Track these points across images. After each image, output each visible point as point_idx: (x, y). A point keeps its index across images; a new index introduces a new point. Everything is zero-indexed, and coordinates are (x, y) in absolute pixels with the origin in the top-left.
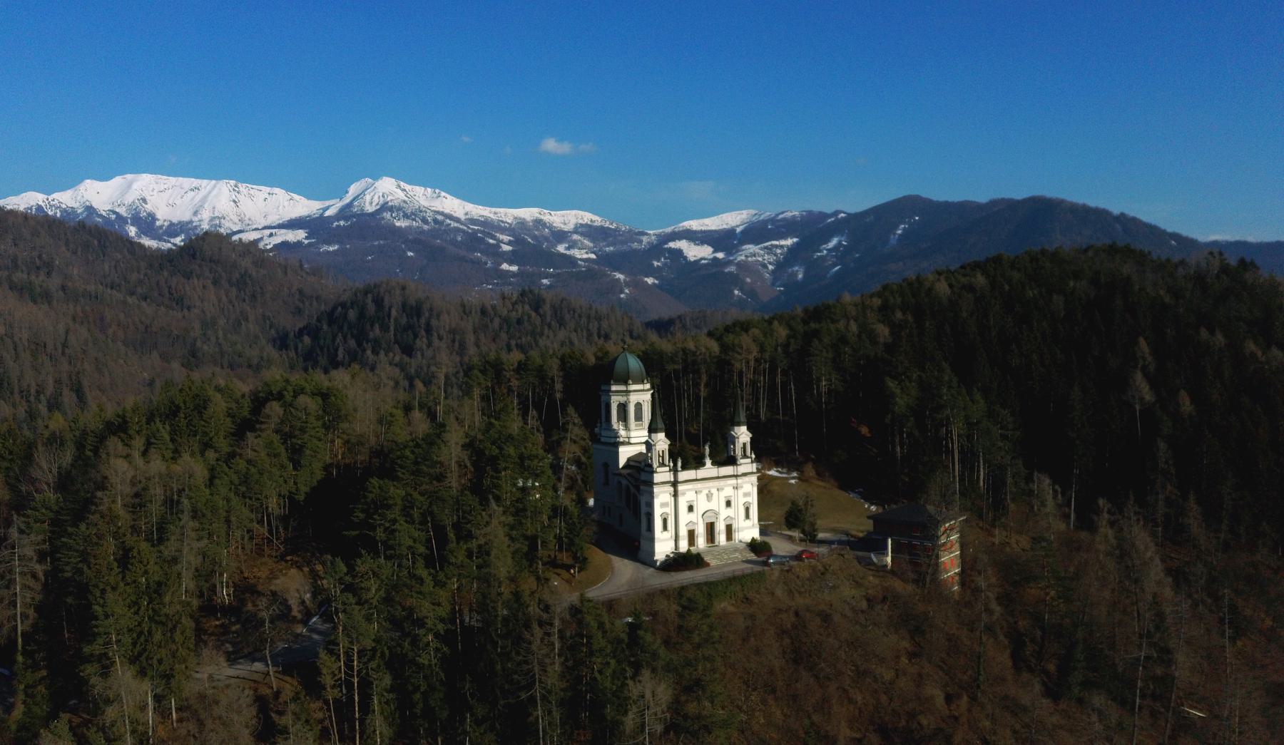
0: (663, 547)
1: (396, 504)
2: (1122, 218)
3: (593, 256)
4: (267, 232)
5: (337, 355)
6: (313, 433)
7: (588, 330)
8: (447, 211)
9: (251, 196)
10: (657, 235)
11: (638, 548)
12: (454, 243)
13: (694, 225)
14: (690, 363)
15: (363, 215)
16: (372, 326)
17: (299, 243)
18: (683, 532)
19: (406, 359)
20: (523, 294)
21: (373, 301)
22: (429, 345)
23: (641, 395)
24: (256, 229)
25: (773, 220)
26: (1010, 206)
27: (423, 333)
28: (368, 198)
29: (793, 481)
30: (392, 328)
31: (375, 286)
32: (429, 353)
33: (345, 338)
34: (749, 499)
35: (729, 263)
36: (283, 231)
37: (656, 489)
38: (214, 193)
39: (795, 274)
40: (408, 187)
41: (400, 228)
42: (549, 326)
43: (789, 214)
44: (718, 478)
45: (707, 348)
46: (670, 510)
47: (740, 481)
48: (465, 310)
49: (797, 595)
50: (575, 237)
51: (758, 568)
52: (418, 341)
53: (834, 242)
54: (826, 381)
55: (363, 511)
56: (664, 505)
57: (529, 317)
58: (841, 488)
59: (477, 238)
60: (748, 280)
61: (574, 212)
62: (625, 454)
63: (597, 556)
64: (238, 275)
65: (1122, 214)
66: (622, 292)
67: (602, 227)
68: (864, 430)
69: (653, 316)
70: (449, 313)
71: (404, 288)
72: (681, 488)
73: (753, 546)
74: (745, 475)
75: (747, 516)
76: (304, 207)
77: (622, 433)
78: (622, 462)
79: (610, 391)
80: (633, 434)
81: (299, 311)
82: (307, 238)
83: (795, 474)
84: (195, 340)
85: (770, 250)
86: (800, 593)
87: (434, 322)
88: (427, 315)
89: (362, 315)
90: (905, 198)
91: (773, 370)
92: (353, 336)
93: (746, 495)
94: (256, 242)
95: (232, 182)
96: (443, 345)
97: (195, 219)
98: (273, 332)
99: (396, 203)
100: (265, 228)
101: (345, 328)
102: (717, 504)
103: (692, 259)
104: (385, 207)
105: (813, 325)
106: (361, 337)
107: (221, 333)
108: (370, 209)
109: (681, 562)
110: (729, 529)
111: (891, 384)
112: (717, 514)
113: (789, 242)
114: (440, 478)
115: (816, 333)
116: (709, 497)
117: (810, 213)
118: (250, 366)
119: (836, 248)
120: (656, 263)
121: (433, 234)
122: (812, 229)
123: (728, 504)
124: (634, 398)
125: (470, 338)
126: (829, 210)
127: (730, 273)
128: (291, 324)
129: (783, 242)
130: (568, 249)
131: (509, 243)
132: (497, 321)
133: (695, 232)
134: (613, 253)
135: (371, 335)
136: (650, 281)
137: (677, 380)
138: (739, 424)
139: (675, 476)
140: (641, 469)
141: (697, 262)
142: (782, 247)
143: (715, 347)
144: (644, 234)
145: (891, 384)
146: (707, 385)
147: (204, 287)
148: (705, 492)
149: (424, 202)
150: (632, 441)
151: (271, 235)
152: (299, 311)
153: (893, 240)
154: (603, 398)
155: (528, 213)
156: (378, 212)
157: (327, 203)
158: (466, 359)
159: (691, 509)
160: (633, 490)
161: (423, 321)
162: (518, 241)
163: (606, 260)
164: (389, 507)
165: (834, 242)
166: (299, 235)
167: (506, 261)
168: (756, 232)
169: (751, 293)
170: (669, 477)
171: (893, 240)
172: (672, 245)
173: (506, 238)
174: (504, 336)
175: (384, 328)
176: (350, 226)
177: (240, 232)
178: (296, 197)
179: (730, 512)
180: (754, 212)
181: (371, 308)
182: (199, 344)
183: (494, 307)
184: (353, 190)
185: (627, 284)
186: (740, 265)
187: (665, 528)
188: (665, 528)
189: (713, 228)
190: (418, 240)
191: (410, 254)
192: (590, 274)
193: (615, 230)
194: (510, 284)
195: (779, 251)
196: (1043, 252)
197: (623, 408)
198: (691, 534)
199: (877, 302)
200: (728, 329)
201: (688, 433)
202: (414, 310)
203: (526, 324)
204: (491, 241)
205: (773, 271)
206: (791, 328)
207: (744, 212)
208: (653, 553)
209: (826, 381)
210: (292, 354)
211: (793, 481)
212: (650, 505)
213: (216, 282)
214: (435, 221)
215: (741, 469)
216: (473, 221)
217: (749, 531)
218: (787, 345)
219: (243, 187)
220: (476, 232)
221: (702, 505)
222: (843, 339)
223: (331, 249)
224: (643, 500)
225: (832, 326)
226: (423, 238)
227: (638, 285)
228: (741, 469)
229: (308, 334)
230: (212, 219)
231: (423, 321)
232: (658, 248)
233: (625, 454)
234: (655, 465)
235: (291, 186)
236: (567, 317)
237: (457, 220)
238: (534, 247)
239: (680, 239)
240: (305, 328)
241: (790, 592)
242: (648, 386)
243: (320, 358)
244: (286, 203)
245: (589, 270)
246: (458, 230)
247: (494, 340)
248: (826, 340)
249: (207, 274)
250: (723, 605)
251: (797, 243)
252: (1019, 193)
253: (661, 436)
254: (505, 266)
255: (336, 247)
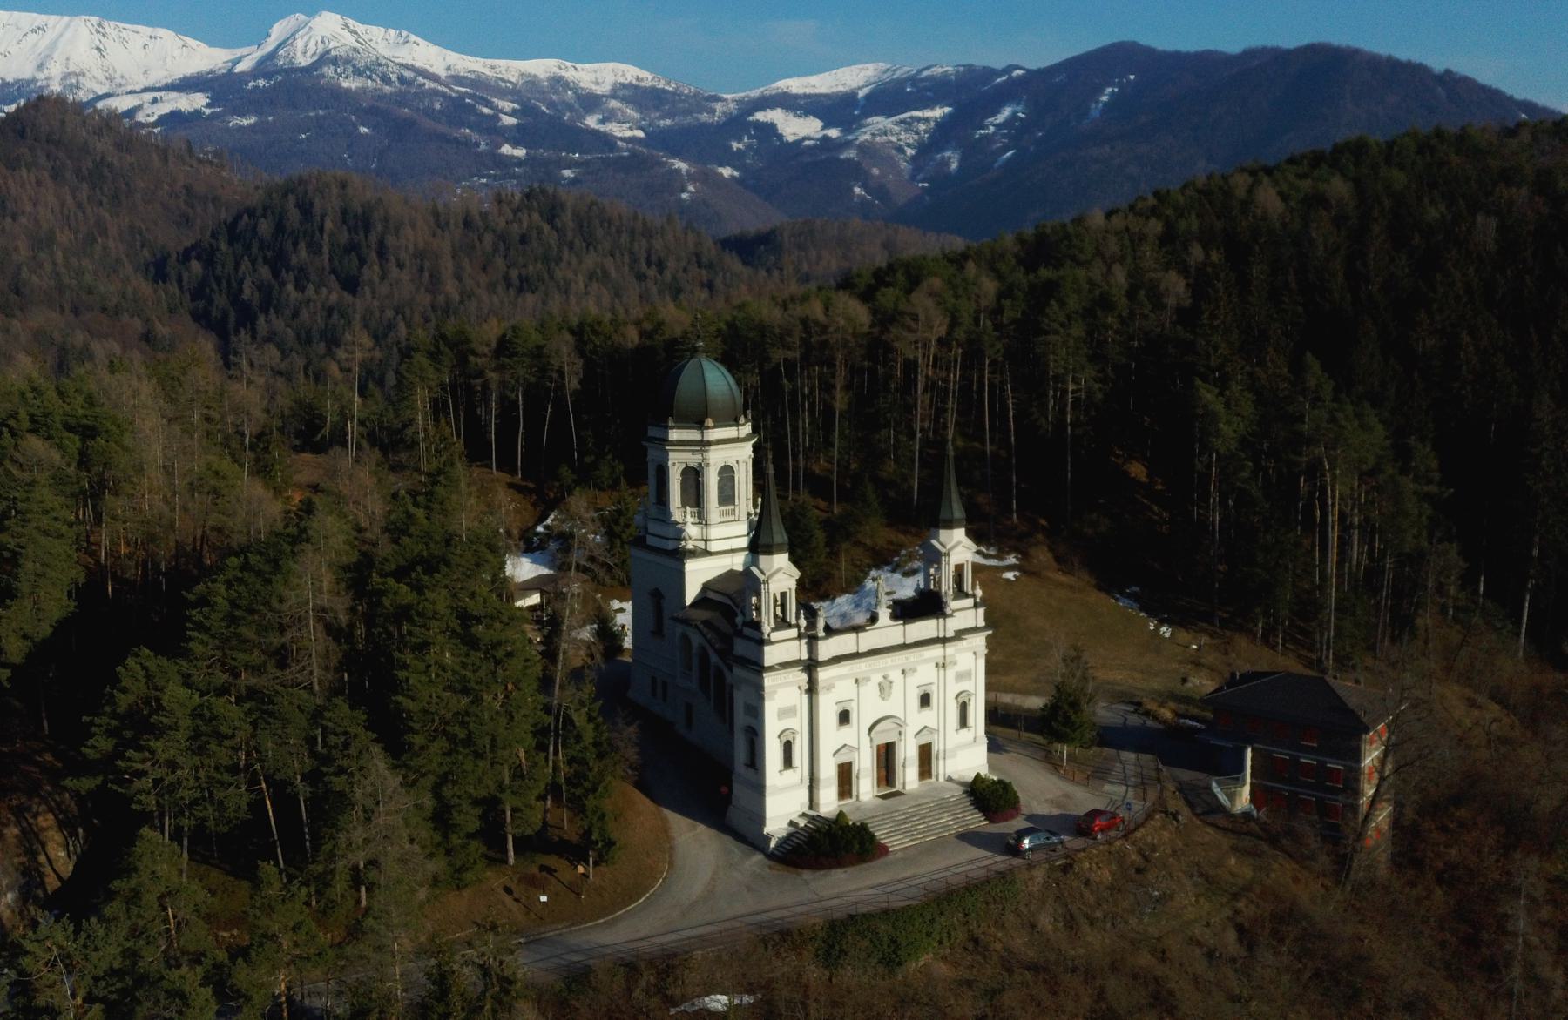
0: (784, 805)
1: (175, 727)
2: (1449, 81)
3: (640, 134)
4: (149, 96)
5: (241, 291)
6: (45, 522)
7: (631, 253)
8: (418, 64)
9: (124, 41)
10: (737, 102)
11: (727, 800)
12: (429, 113)
13: (795, 85)
14: (816, 347)
15: (292, 70)
16: (295, 244)
17: (197, 114)
18: (828, 772)
19: (348, 298)
20: (528, 196)
21: (297, 206)
22: (383, 278)
23: (731, 450)
24: (132, 92)
25: (913, 80)
26: (1278, 57)
27: (374, 256)
28: (300, 44)
29: (1010, 575)
30: (326, 250)
31: (301, 181)
32: (384, 289)
33: (253, 263)
34: (967, 685)
35: (847, 144)
36: (173, 95)
37: (769, 680)
38: (68, 35)
39: (946, 163)
40: (360, 28)
41: (348, 90)
42: (571, 246)
43: (937, 71)
44: (904, 647)
45: (849, 319)
46: (799, 723)
47: (951, 649)
48: (439, 221)
49: (1086, 928)
50: (613, 103)
51: (999, 861)
52: (365, 270)
53: (1006, 113)
54: (1075, 377)
55: (110, 733)
56: (784, 713)
57: (540, 231)
58: (1100, 589)
59: (464, 106)
60: (876, 171)
61: (611, 65)
62: (697, 575)
63: (639, 817)
64: (90, 164)
65: (1448, 72)
66: (684, 190)
67: (653, 90)
68: (1137, 470)
69: (732, 229)
70: (413, 226)
71: (343, 185)
72: (823, 674)
73: (986, 796)
74: (960, 635)
75: (963, 722)
76: (205, 58)
77: (692, 531)
78: (691, 592)
79: (665, 441)
80: (714, 532)
81: (186, 221)
82: (208, 106)
83: (1012, 560)
84: (19, 267)
85: (908, 125)
86: (1092, 923)
87: (390, 240)
88: (379, 227)
89: (280, 227)
90: (1113, 45)
91: (973, 354)
92: (266, 261)
93: (961, 677)
94: (131, 113)
95: (95, 20)
96: (405, 276)
97: (40, 76)
98: (146, 252)
99: (342, 52)
100: (146, 90)
101: (255, 250)
102: (902, 702)
103: (791, 139)
104: (325, 59)
105: (1045, 273)
106: (278, 263)
107: (59, 256)
108: (303, 61)
109: (830, 843)
110: (926, 755)
111: (1208, 395)
112: (901, 726)
113: (938, 113)
114: (282, 657)
115: (1050, 290)
116: (884, 688)
117: (970, 68)
118: (104, 310)
119: (1007, 124)
120: (735, 145)
121: (401, 99)
122: (972, 94)
123: (925, 700)
124: (717, 458)
125: (447, 267)
126: (999, 65)
127: (848, 160)
128: (173, 239)
129: (928, 113)
130: (602, 122)
131: (513, 113)
132: (488, 239)
133: (797, 97)
134: (669, 129)
135: (294, 260)
136: (726, 172)
137: (791, 379)
138: (950, 525)
139: (812, 649)
140: (732, 600)
141: (798, 143)
142: (927, 120)
143: (861, 314)
144: (716, 99)
145: (1208, 395)
146: (847, 387)
147: (39, 183)
148: (878, 678)
149: (384, 51)
150: (713, 547)
151: (155, 101)
152: (186, 221)
153: (1095, 110)
154: (652, 454)
155: (542, 68)
156: (315, 66)
157: (239, 52)
158: (441, 299)
159: (844, 717)
160: (714, 658)
161: (373, 237)
162: (525, 110)
163: (658, 139)
164: (158, 732)
165: (1006, 113)
166: (197, 102)
167: (507, 141)
168: (888, 98)
169: (879, 191)
170: (799, 650)
171: (1095, 110)
172: (760, 116)
173: (507, 105)
174: (499, 262)
175: (314, 248)
176: (274, 88)
177: (107, 96)
178: (191, 42)
179: (928, 717)
180: (883, 66)
181: (294, 216)
182: (25, 274)
183: (484, 216)
184: (278, 31)
185: (692, 178)
186: (864, 149)
187: (788, 762)
188: (788, 762)
189: (823, 90)
190: (376, 110)
191: (363, 130)
192: (635, 162)
193: (674, 93)
194: (514, 176)
195: (922, 127)
196: (1439, 134)
197: (694, 478)
198: (845, 775)
199: (1155, 227)
200: (882, 277)
201: (809, 475)
202: (359, 221)
203: (535, 244)
204: (486, 110)
205: (913, 158)
206: (1000, 277)
207: (871, 66)
208: (760, 819)
209: (1075, 377)
210: (173, 289)
211: (1010, 575)
212: (756, 711)
213: (56, 175)
214: (401, 79)
215: (952, 625)
216: (458, 80)
217: (967, 756)
218: (997, 311)
219: (110, 27)
220: (462, 96)
221: (868, 708)
222: (1105, 303)
223: (245, 122)
224: (740, 699)
225: (1081, 273)
226: (382, 105)
227: (706, 178)
228: (952, 625)
229: (198, 258)
230: (66, 76)
231: (373, 237)
232: (738, 122)
233: (697, 575)
234: (767, 626)
235: (180, 29)
236: (599, 233)
237: (434, 78)
238: (550, 121)
239: (772, 107)
240: (193, 247)
241: (1070, 923)
242: (746, 429)
243: (216, 296)
244: (177, 53)
245: (634, 155)
246: (435, 93)
247: (484, 269)
248: (1073, 303)
249: (42, 160)
250: (928, 963)
251: (950, 114)
252: (1290, 38)
253: (781, 560)
254: (506, 149)
255: (253, 120)
